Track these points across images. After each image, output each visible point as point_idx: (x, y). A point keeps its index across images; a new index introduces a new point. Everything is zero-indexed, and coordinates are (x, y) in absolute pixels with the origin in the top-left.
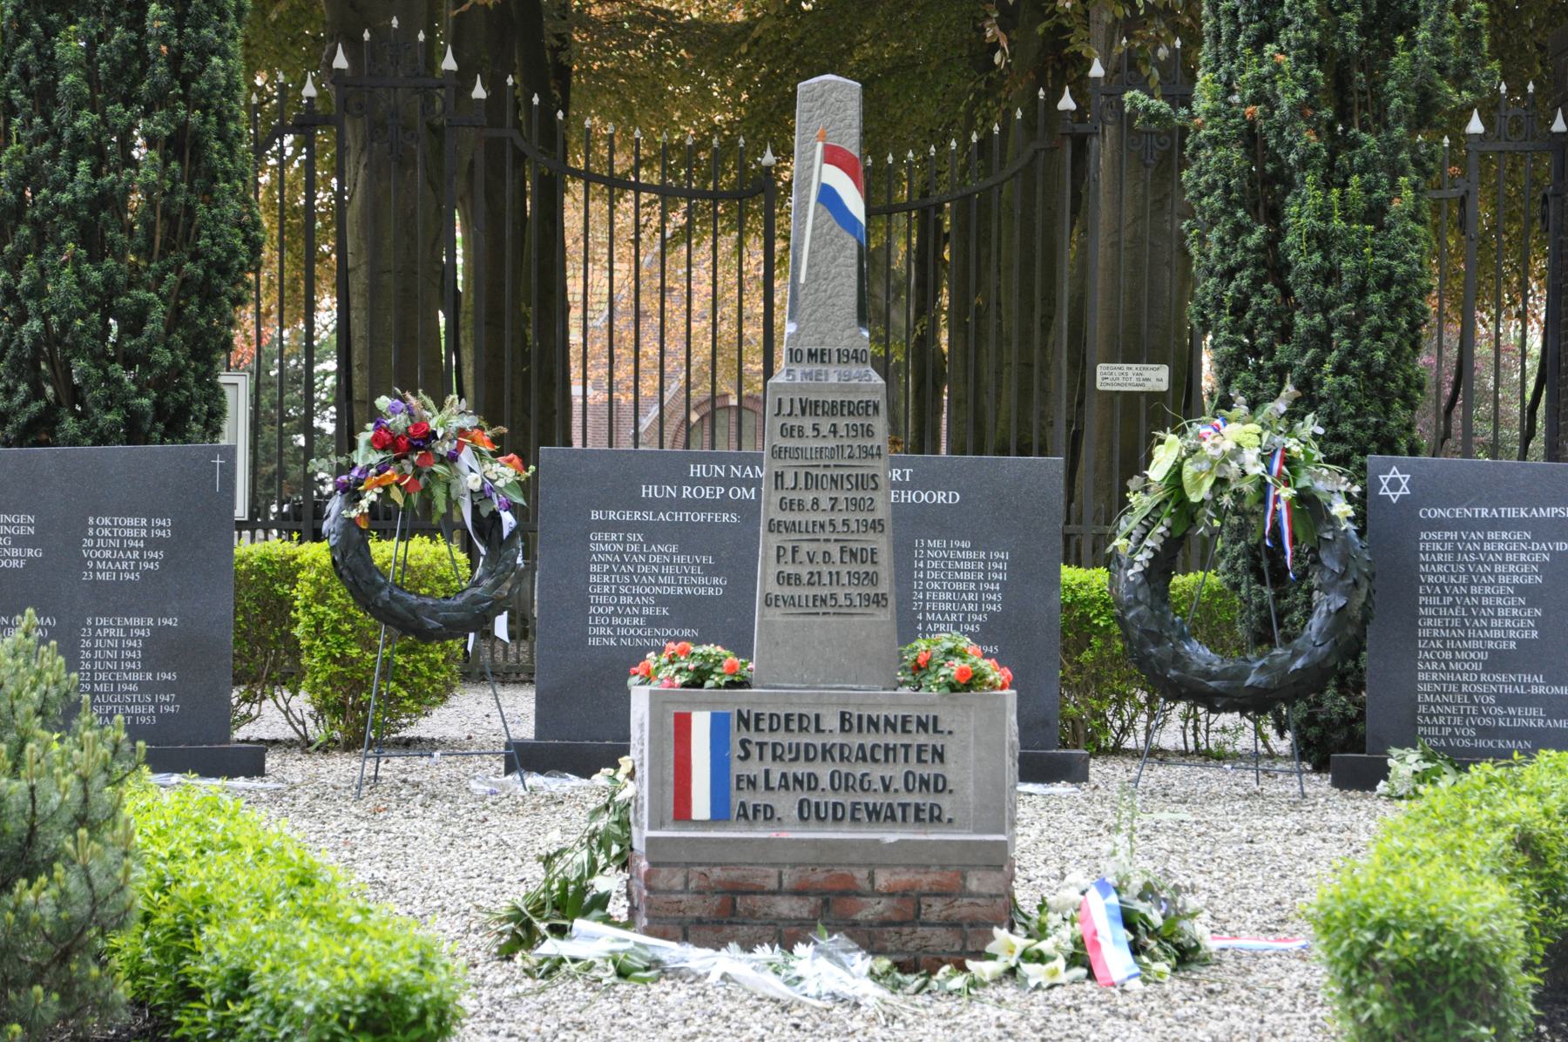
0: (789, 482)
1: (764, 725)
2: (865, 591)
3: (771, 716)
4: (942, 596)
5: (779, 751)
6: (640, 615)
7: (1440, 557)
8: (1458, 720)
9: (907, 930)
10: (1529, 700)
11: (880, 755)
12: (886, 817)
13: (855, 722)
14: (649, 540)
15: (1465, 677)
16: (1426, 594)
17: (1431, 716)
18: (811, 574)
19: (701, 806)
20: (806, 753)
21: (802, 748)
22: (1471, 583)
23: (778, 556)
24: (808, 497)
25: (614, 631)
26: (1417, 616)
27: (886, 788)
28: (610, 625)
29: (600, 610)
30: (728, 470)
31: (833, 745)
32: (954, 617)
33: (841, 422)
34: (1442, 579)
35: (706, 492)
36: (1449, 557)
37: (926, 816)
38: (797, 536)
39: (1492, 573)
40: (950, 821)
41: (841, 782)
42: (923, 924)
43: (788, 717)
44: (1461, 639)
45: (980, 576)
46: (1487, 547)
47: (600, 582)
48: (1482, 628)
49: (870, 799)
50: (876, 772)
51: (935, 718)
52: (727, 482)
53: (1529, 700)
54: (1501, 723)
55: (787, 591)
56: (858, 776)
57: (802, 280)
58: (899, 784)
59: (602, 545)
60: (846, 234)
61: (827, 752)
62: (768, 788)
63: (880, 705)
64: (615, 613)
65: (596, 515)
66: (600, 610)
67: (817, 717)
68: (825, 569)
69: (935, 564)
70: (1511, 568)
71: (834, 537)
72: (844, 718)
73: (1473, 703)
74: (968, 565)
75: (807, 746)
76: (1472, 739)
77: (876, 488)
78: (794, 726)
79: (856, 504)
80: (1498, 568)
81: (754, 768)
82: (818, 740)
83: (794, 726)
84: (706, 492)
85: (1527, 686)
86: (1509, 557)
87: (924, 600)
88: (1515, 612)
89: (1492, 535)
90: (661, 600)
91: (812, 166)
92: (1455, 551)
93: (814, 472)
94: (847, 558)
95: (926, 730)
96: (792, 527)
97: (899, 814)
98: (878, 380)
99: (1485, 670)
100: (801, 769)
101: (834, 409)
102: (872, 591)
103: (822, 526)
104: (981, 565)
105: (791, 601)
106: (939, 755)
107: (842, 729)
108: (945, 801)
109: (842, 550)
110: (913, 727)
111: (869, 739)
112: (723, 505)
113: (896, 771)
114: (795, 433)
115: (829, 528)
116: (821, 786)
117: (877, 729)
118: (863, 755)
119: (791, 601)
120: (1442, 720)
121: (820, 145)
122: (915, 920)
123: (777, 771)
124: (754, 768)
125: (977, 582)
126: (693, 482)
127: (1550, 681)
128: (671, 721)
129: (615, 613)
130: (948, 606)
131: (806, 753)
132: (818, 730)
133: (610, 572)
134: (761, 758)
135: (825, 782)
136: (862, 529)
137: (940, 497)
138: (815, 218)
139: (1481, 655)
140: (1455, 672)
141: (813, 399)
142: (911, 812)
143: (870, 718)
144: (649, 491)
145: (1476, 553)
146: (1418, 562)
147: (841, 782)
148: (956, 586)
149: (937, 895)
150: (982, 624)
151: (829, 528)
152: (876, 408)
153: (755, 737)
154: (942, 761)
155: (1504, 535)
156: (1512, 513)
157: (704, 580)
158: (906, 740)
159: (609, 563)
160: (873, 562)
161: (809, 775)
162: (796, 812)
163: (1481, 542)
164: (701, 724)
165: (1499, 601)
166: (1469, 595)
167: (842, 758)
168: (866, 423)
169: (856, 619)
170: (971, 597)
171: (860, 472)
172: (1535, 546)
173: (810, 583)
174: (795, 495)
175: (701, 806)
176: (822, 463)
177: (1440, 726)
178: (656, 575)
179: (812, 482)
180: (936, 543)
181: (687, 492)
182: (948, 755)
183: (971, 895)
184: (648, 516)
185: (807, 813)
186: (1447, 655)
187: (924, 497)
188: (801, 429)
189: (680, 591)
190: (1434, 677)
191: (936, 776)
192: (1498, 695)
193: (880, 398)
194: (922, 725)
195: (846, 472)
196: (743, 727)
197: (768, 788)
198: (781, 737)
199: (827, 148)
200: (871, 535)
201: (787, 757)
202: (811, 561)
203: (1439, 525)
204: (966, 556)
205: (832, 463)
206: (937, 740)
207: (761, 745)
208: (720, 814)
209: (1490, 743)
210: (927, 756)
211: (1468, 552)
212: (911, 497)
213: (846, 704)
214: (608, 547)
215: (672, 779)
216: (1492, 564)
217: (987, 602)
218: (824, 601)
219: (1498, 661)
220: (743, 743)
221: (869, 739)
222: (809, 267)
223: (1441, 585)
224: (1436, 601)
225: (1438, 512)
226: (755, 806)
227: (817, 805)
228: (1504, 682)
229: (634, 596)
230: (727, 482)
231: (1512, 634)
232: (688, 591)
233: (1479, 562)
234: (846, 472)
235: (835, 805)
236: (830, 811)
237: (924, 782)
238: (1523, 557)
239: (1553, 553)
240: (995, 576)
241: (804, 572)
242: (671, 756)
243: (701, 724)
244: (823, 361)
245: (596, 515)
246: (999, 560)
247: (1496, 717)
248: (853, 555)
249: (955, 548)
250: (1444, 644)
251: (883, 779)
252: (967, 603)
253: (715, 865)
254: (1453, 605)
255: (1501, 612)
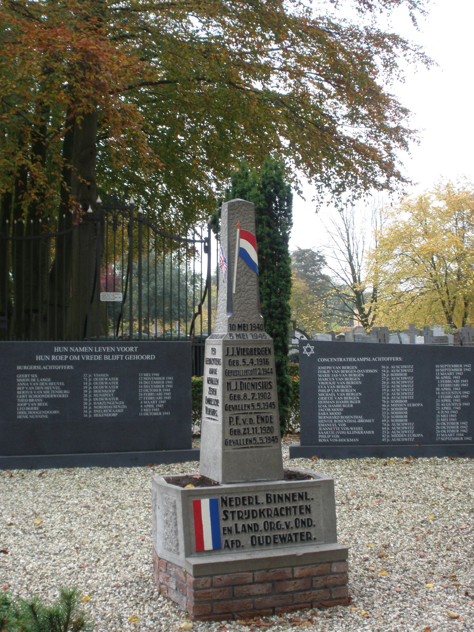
0: (233, 387)
1: (233, 503)
2: (268, 435)
3: (236, 498)
4: (149, 394)
5: (241, 514)
6: (37, 406)
7: (325, 376)
8: (333, 433)
9: (308, 593)
10: (358, 425)
11: (284, 512)
12: (289, 540)
13: (272, 498)
14: (40, 377)
15: (335, 417)
16: (321, 389)
17: (323, 431)
18: (245, 429)
19: (208, 544)
20: (251, 515)
21: (251, 512)
22: (336, 384)
23: (230, 422)
24: (242, 393)
25: (27, 412)
26: (318, 396)
27: (288, 527)
28: (25, 410)
29: (22, 405)
30: (69, 349)
31: (264, 510)
32: (154, 402)
33: (255, 358)
34: (327, 383)
35: (61, 358)
36: (329, 375)
37: (305, 538)
38: (238, 412)
39: (344, 381)
40: (315, 538)
41: (269, 526)
42: (314, 589)
43: (243, 498)
44: (333, 404)
45: (163, 386)
46: (342, 372)
47: (21, 393)
48: (341, 400)
49: (281, 533)
50: (283, 520)
51: (306, 493)
52: (69, 353)
53: (358, 425)
54: (348, 433)
55: (234, 438)
56: (275, 522)
57: (234, 292)
58: (293, 525)
59: (22, 379)
60: (251, 271)
61: (261, 512)
62: (237, 532)
63: (282, 489)
64: (27, 406)
65: (19, 368)
66: (22, 405)
67: (256, 497)
68: (250, 426)
69: (146, 383)
70: (351, 379)
71: (253, 411)
72: (268, 497)
73: (338, 426)
74: (157, 382)
75: (253, 511)
76: (338, 439)
77: (271, 388)
78: (246, 502)
79: (262, 396)
80: (346, 379)
81: (230, 524)
82: (257, 508)
83: (246, 502)
84: (61, 358)
85: (357, 420)
86: (350, 375)
87: (143, 396)
88: (352, 394)
89: (343, 367)
90: (45, 400)
91: (235, 240)
92: (331, 373)
93: (244, 381)
94: (260, 421)
95: (302, 499)
96: (235, 408)
97: (294, 538)
98: (269, 338)
99: (342, 415)
100: (251, 522)
101: (251, 352)
102: (270, 435)
103: (249, 407)
104: (163, 382)
105: (236, 443)
106: (308, 509)
107: (267, 502)
108: (312, 530)
109: (258, 418)
110: (297, 498)
111: (279, 506)
112: (68, 362)
113: (291, 519)
114: (235, 364)
115: (251, 408)
116: (260, 529)
117: (282, 500)
118: (278, 513)
119: (236, 443)
120: (327, 433)
121: (238, 230)
122: (312, 588)
123: (240, 524)
124: (230, 524)
125: (162, 389)
126: (56, 354)
127: (365, 418)
128: (191, 505)
129: (27, 406)
130: (152, 398)
131: (251, 515)
132: (257, 503)
133: (25, 390)
134: (233, 518)
135: (261, 527)
136: (266, 407)
137: (148, 357)
138: (238, 263)
139: (340, 409)
140: (332, 416)
141: (242, 347)
142: (299, 537)
143: (278, 495)
144: (39, 358)
145: (338, 374)
146: (317, 377)
147: (269, 526)
148: (154, 390)
149: (319, 576)
150: (164, 404)
151: (251, 408)
152: (270, 351)
153: (230, 509)
154: (310, 512)
155: (348, 367)
156: (350, 359)
157: (61, 392)
158: (294, 505)
159: (24, 386)
160: (271, 422)
161: (255, 524)
162: (250, 542)
163: (340, 370)
164: (205, 504)
165: (347, 391)
166: (336, 389)
167: (268, 515)
168: (266, 358)
169: (265, 449)
170: (160, 394)
171: (264, 381)
172: (359, 371)
173: (244, 434)
174: (236, 393)
175: (208, 544)
176: (247, 377)
177: (327, 435)
178: (42, 390)
179: (243, 386)
180: (146, 375)
181: (53, 358)
182: (312, 509)
183: (333, 573)
184: (39, 368)
185: (256, 543)
186: (329, 410)
187: (142, 357)
188: (237, 362)
189: (52, 396)
190: (324, 417)
191: (308, 519)
192: (347, 423)
193: (271, 346)
194: (301, 497)
195: (257, 381)
196: (224, 505)
197: (237, 532)
198: (241, 508)
199: (241, 231)
200: (269, 410)
201: (245, 517)
202: (244, 423)
203: (325, 364)
204: (158, 379)
205: (251, 377)
206: (307, 503)
207: (233, 512)
208: (217, 546)
209: (344, 440)
210: (304, 511)
211: (335, 374)
212: (137, 357)
213: (268, 490)
214: (24, 380)
215: (194, 532)
216: (344, 378)
217: (166, 396)
218: (250, 441)
219: (346, 411)
220: (225, 512)
221: (279, 506)
222: (237, 286)
223: (326, 385)
224: (324, 391)
225: (325, 360)
226: (232, 541)
227: (259, 537)
228: (349, 419)
229: (34, 399)
230: (69, 353)
231: (351, 402)
232: (55, 396)
233: (339, 377)
234: (261, 381)
235: (267, 537)
236: (265, 540)
237: (303, 522)
238: (355, 375)
239: (365, 374)
240: (168, 386)
241: (241, 428)
242: (193, 521)
243: (205, 504)
244: (244, 330)
245: (19, 368)
246: (170, 380)
247: (346, 431)
248: (262, 419)
249: (154, 376)
250: (327, 406)
251: (286, 523)
252: (158, 396)
253: (224, 574)
254: (330, 392)
255: (347, 394)
